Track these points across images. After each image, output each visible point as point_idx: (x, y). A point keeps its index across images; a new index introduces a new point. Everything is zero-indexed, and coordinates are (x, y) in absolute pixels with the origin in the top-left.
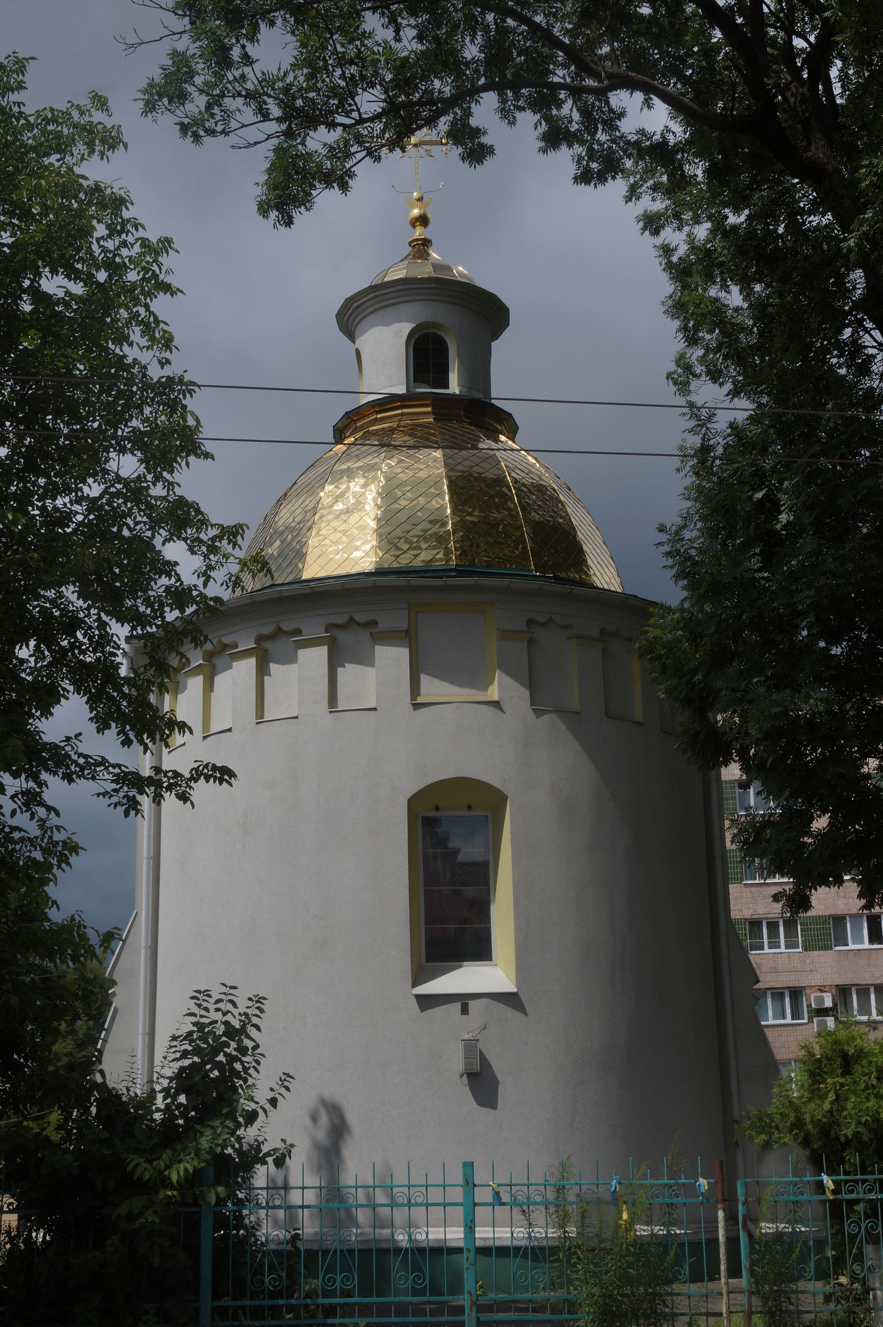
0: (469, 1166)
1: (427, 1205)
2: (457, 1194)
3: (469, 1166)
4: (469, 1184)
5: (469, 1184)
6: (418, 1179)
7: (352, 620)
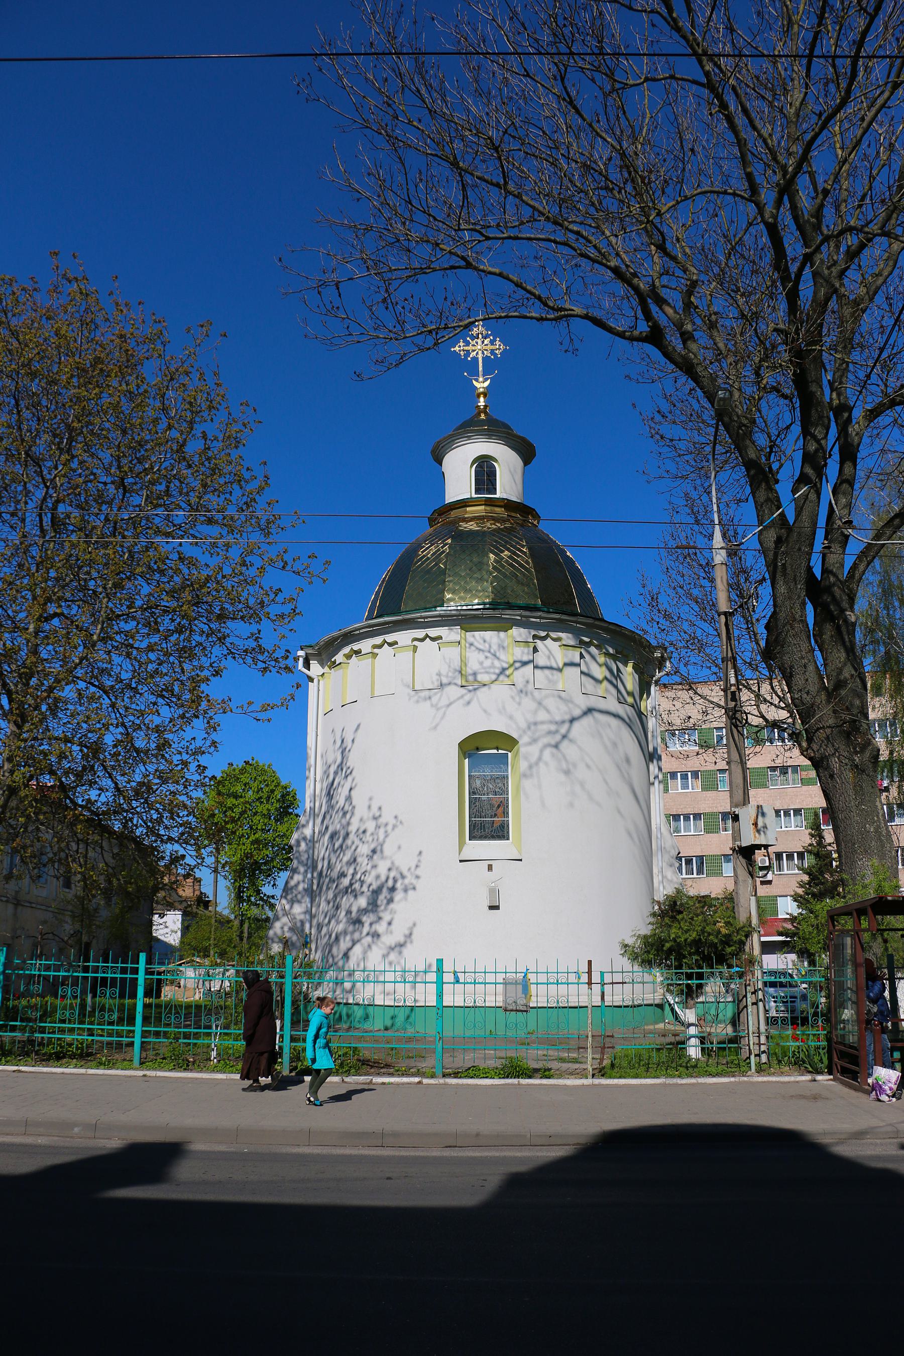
1: (485, 984)
5: (440, 971)
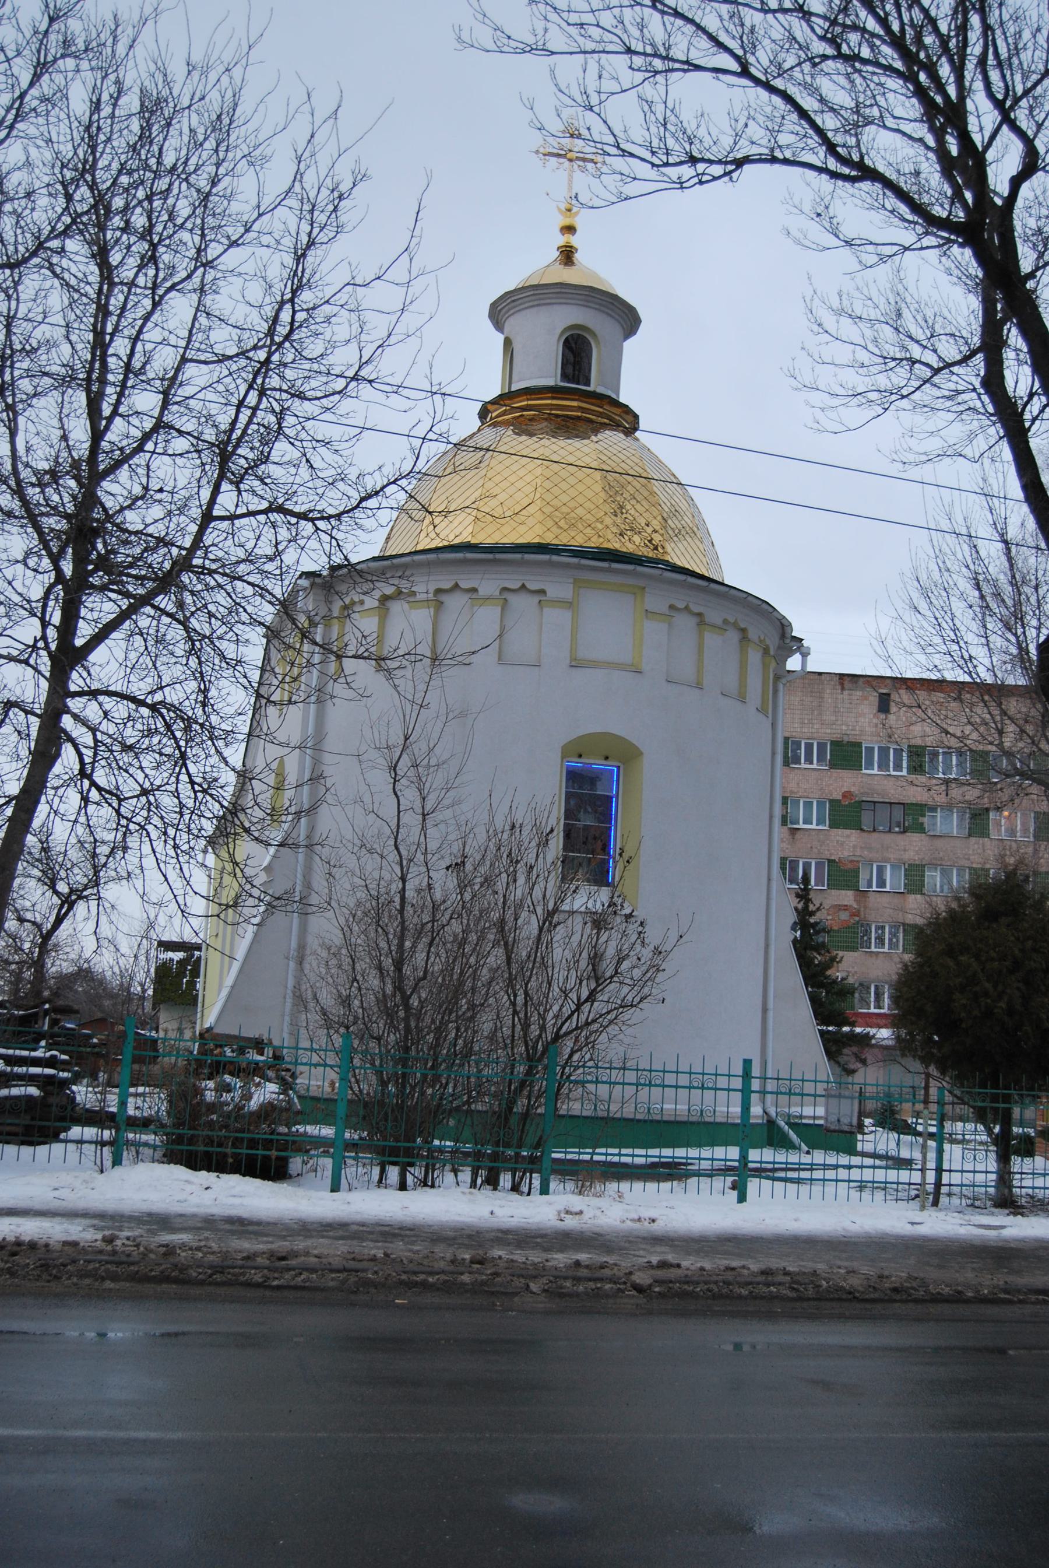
0: (747, 1063)
2: (737, 1083)
3: (747, 1063)
4: (747, 1075)
5: (747, 1075)
6: (797, 1075)
7: (523, 586)
